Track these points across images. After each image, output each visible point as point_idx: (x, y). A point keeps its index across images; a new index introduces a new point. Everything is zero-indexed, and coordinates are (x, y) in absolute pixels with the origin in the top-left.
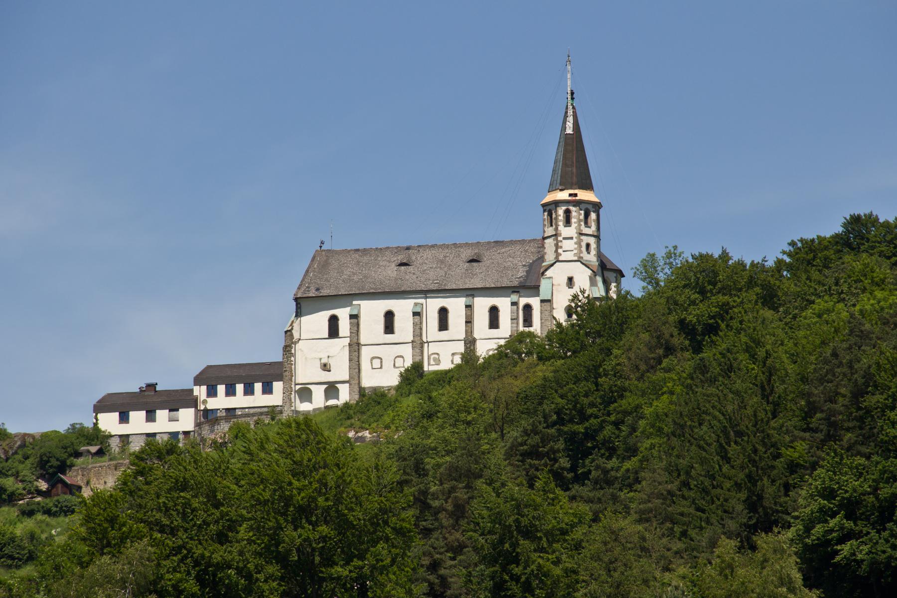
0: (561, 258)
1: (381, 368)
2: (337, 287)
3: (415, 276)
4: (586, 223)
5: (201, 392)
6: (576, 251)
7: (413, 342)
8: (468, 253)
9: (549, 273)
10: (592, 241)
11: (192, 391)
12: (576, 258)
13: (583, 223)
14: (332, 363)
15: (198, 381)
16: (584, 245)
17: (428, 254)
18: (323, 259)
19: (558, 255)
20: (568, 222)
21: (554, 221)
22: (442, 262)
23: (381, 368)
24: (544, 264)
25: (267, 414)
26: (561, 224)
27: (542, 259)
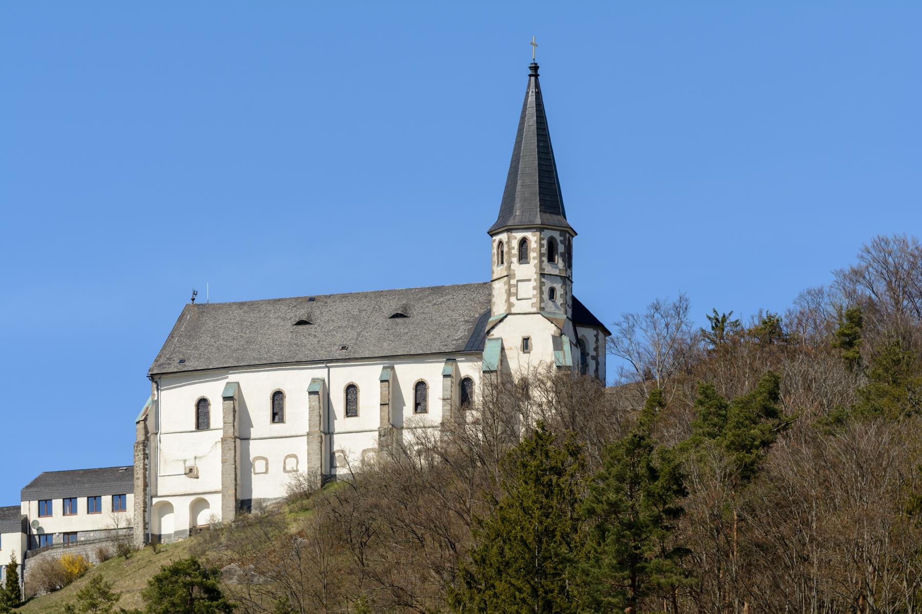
0: (513, 310)
1: (266, 472)
2: (209, 359)
3: (316, 340)
4: (551, 259)
5: (30, 509)
6: (534, 300)
7: (308, 434)
8: (393, 306)
9: (496, 333)
10: (559, 288)
11: (19, 508)
12: (534, 310)
13: (545, 259)
14: (201, 466)
15: (27, 494)
16: (546, 290)
17: (341, 307)
18: (197, 313)
19: (510, 305)
20: (523, 257)
21: (505, 257)
22: (355, 318)
23: (266, 472)
24: (491, 319)
25: (107, 539)
26: (515, 260)
27: (488, 313)
